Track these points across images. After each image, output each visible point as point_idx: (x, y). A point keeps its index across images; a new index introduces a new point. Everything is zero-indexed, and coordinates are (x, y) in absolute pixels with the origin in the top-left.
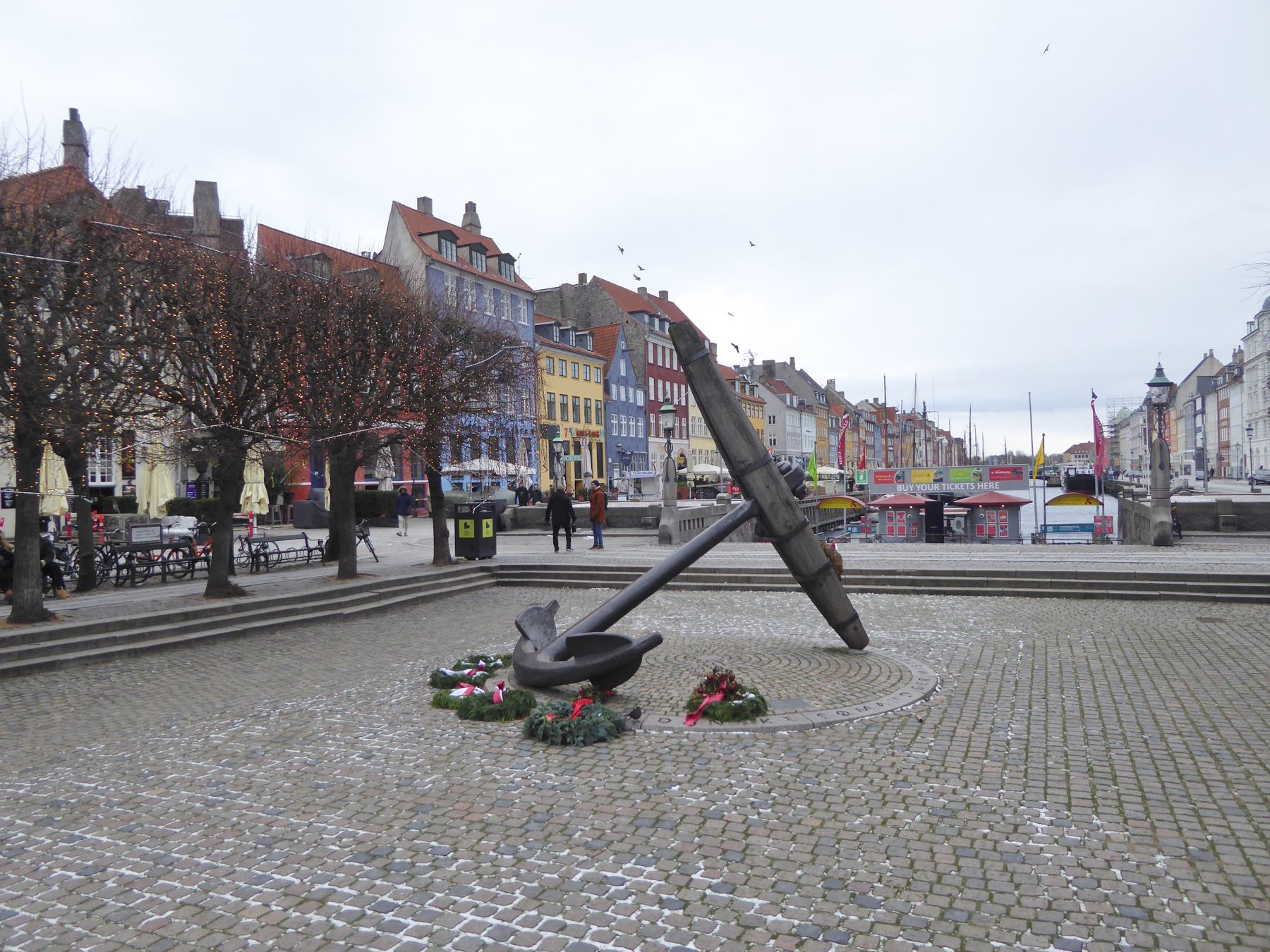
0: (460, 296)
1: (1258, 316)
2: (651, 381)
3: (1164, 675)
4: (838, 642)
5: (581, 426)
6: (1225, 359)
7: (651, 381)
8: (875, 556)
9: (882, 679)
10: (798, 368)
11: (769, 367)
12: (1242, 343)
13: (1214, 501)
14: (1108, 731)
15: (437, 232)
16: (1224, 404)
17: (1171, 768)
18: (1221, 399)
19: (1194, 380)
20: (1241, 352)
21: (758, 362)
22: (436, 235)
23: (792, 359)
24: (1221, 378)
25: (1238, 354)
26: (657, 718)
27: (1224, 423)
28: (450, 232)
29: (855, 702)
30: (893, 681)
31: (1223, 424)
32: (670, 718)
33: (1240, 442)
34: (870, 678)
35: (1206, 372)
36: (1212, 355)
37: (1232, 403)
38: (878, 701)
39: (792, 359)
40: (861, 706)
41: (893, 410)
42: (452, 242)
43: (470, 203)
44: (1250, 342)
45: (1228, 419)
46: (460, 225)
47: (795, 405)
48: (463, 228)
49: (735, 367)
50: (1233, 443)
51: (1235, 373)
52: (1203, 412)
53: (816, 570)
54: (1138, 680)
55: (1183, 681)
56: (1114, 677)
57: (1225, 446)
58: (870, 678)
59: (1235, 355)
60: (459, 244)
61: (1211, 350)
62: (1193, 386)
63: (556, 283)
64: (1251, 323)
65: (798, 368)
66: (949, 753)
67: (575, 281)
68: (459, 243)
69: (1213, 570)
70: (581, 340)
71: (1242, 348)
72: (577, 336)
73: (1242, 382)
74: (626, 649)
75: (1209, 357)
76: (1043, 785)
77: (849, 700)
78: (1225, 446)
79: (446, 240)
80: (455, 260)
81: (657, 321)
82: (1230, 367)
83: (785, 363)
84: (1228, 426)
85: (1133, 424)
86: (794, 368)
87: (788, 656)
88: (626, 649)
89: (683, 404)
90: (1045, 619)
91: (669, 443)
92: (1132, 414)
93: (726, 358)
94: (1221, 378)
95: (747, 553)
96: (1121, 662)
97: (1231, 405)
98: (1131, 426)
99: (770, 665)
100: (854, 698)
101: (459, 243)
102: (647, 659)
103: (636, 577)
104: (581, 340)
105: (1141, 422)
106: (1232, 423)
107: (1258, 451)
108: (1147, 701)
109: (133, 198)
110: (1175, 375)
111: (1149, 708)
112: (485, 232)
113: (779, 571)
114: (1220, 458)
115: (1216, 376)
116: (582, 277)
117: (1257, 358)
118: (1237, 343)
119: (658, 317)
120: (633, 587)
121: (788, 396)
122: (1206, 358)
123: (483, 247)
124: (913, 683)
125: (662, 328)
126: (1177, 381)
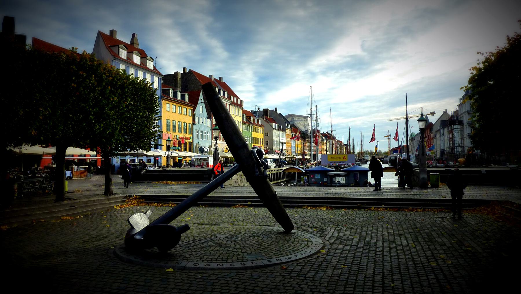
0: (152, 84)
3: (419, 242)
5: (181, 135)
8: (169, 188)
9: (299, 244)
10: (278, 112)
11: (266, 111)
13: (444, 169)
14: (393, 266)
17: (418, 281)
19: (439, 121)
21: (261, 109)
23: (276, 108)
26: (193, 263)
29: (285, 255)
30: (304, 245)
32: (199, 263)
34: (293, 245)
35: (446, 119)
36: (446, 111)
38: (295, 254)
39: (276, 108)
40: (287, 257)
47: (277, 128)
49: (251, 111)
52: (443, 135)
54: (408, 244)
55: (427, 244)
56: (398, 243)
58: (293, 245)
61: (446, 110)
62: (439, 124)
64: (461, 99)
65: (278, 112)
66: (323, 277)
69: (236, 195)
71: (458, 109)
76: (362, 290)
77: (270, 254)
85: (416, 140)
86: (277, 112)
87: (258, 235)
90: (373, 218)
91: (216, 142)
92: (416, 135)
95: (321, 190)
96: (403, 236)
99: (249, 239)
100: (284, 253)
108: (411, 253)
109: (431, 123)
110: (433, 120)
111: (411, 256)
113: (254, 197)
121: (274, 124)
122: (444, 113)
124: (312, 246)
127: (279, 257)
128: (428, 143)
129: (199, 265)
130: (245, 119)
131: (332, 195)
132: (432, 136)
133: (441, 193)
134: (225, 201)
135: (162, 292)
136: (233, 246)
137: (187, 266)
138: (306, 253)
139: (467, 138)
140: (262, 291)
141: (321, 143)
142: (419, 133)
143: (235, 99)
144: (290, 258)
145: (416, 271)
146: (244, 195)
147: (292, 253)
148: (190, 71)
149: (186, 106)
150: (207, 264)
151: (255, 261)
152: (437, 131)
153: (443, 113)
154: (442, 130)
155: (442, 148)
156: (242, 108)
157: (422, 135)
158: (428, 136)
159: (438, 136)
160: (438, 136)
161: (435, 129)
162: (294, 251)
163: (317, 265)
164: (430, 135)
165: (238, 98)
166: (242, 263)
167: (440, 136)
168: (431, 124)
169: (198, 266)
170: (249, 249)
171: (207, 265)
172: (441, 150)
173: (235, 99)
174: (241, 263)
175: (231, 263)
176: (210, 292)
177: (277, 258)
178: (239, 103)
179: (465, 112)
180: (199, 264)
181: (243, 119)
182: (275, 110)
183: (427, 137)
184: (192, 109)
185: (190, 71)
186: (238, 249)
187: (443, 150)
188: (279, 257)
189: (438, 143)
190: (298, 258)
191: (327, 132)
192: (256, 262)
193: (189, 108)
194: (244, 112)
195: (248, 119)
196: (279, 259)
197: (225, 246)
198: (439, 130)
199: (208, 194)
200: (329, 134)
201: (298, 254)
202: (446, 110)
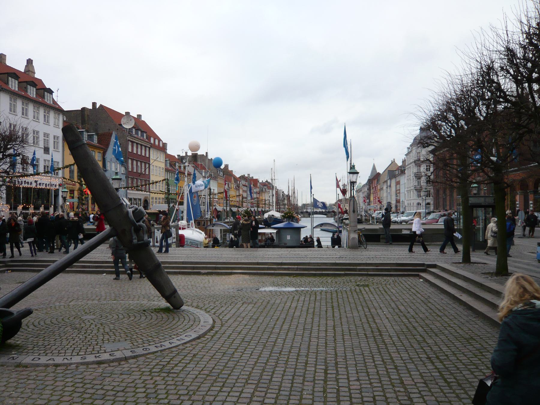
1: (411, 146)
2: (130, 161)
4: (164, 303)
6: (400, 164)
7: (130, 161)
12: (405, 157)
15: (7, 73)
16: (398, 183)
18: (397, 181)
19: (387, 171)
20: (405, 160)
22: (7, 75)
23: (207, 153)
24: (397, 172)
25: (404, 161)
27: (398, 192)
28: (15, 74)
29: (157, 342)
31: (398, 192)
33: (404, 200)
36: (394, 161)
37: (401, 183)
38: (171, 341)
40: (159, 345)
41: (204, 157)
42: (33, 87)
43: (30, 59)
44: (408, 156)
45: (399, 190)
46: (23, 71)
48: (25, 72)
49: (178, 156)
50: (401, 200)
51: (402, 170)
52: (390, 186)
53: (446, 247)
57: (398, 201)
59: (403, 162)
60: (20, 81)
61: (394, 159)
63: (78, 107)
64: (408, 148)
67: (90, 107)
68: (37, 87)
70: (90, 137)
72: (88, 135)
73: (405, 173)
74: (12, 317)
75: (393, 162)
78: (398, 201)
79: (12, 78)
80: (52, 103)
81: (139, 132)
82: (401, 167)
83: (203, 155)
84: (399, 193)
88: (12, 317)
89: (147, 173)
93: (421, 247)
94: (397, 172)
97: (401, 184)
98: (362, 191)
101: (20, 80)
102: (24, 321)
103: (46, 266)
104: (90, 137)
105: (366, 190)
106: (401, 192)
107: (410, 204)
112: (37, 76)
114: (396, 206)
115: (396, 171)
116: (94, 104)
117: (411, 164)
118: (404, 157)
119: (140, 130)
120: (45, 271)
122: (392, 163)
123: (37, 84)
125: (142, 135)
126: (381, 172)
127: (148, 345)
128: (374, 194)
129: (40, 360)
130: (168, 165)
131: (268, 260)
132: (379, 187)
133: (257, 255)
134: (89, 267)
135: (102, 402)
136: (95, 332)
137: (24, 362)
138: (186, 338)
139: (414, 190)
140: (192, 399)
141: (259, 193)
142: (366, 184)
143: (157, 141)
144: (162, 347)
145: (306, 359)
146: (168, 259)
147: (166, 339)
148: (101, 106)
149: (95, 148)
150: (51, 357)
151: (114, 352)
152: (384, 183)
153: (391, 163)
154: (389, 181)
155: (389, 201)
156: (166, 153)
157: (370, 186)
158: (375, 187)
159: (385, 188)
160: (385, 188)
161: (382, 179)
162: (171, 336)
163: (294, 354)
164: (377, 186)
165: (160, 140)
166: (97, 355)
167: (387, 188)
168: (379, 174)
169: (38, 362)
170: (115, 335)
171: (50, 360)
172: (388, 203)
173: (157, 141)
174: (95, 355)
175: (82, 356)
176: (124, 403)
177: (145, 347)
178: (161, 145)
179: (413, 162)
180: (40, 359)
181: (166, 165)
182: (205, 155)
183: (374, 188)
184: (102, 152)
185: (101, 106)
186: (400, 333)
187: (390, 203)
188: (148, 345)
189: (385, 195)
190: (173, 345)
191: (267, 181)
192: (116, 353)
193: (98, 151)
194: (169, 158)
195: (172, 165)
196: (146, 349)
197: (85, 332)
198: (386, 181)
199: (80, 259)
200: (269, 183)
201: (174, 341)
202: (394, 159)
